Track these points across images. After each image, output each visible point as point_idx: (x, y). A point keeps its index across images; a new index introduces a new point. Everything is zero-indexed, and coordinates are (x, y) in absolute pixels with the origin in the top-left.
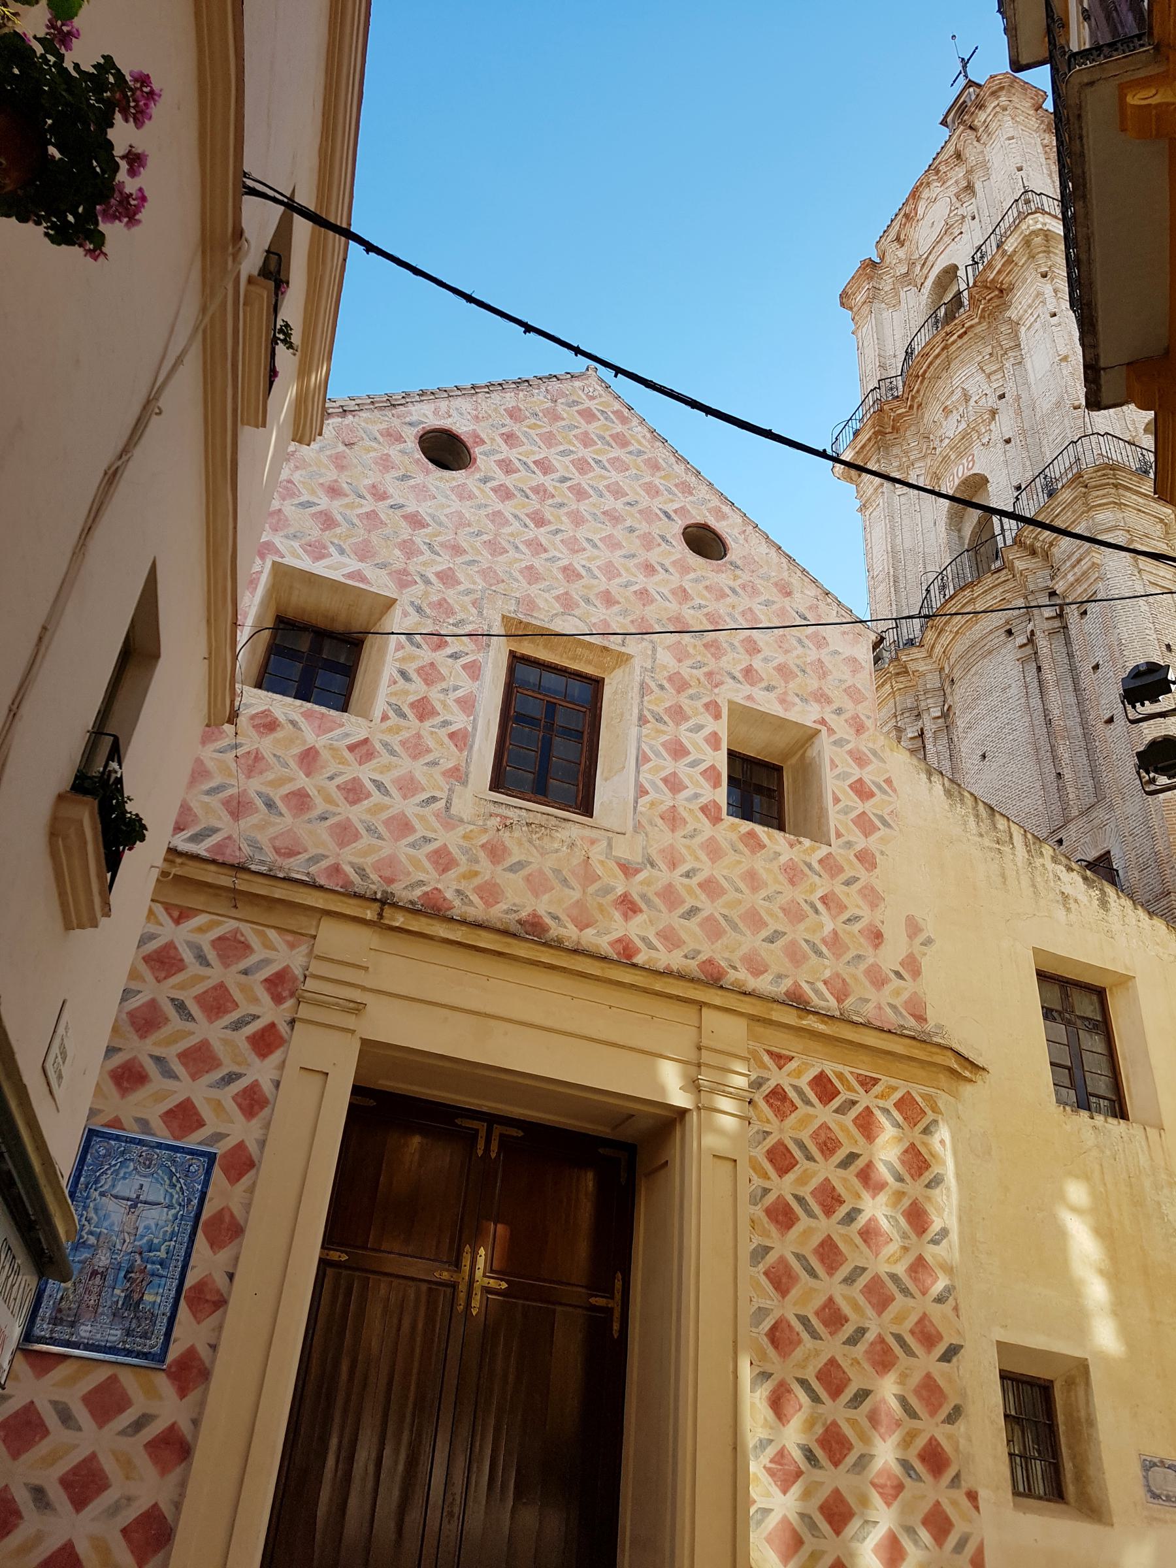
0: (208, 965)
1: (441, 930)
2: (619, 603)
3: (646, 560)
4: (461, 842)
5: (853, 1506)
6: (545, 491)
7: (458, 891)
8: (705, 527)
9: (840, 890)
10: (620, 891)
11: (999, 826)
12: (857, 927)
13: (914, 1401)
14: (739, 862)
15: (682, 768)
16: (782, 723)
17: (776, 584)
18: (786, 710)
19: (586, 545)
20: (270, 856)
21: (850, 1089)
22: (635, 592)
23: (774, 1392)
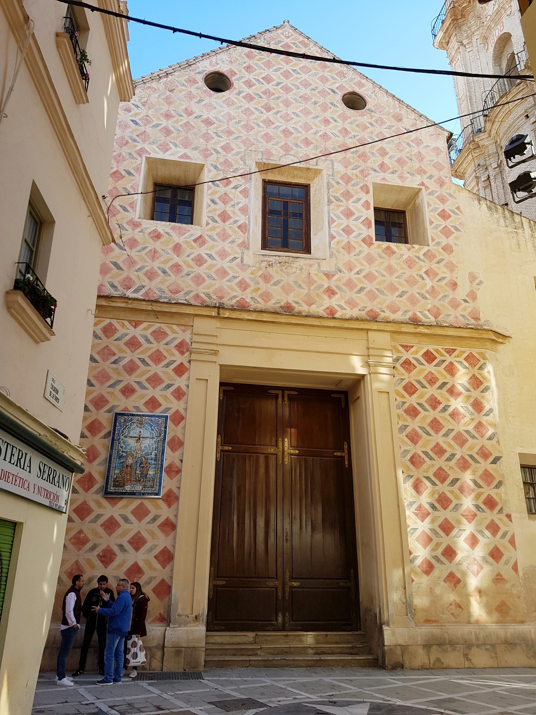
0: (151, 343)
1: (246, 316)
2: (312, 143)
3: (325, 117)
4: (250, 276)
5: (453, 524)
6: (269, 92)
7: (252, 298)
8: (354, 93)
9: (434, 266)
10: (326, 286)
11: (516, 220)
12: (444, 282)
13: (480, 481)
14: (383, 262)
15: (351, 223)
16: (401, 189)
17: (393, 116)
18: (403, 182)
19: (293, 116)
20: (169, 294)
21: (442, 355)
22: (320, 136)
23: (414, 483)
